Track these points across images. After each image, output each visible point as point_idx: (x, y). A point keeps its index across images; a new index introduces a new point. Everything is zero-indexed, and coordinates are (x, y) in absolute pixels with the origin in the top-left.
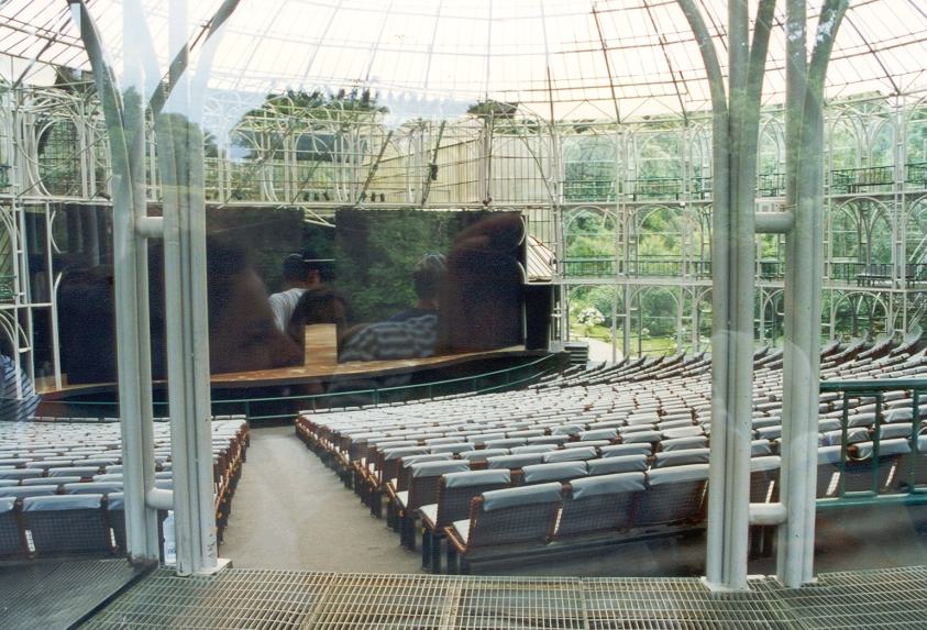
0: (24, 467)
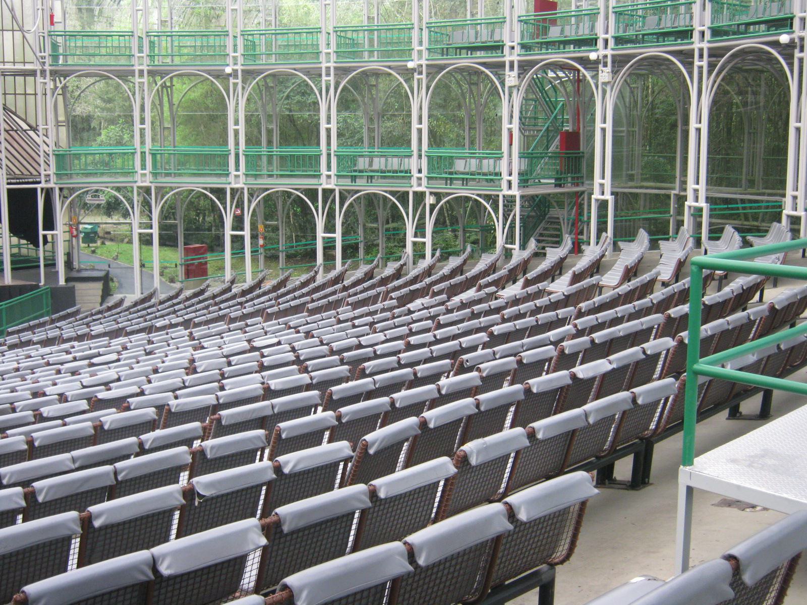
0: (17, 391)
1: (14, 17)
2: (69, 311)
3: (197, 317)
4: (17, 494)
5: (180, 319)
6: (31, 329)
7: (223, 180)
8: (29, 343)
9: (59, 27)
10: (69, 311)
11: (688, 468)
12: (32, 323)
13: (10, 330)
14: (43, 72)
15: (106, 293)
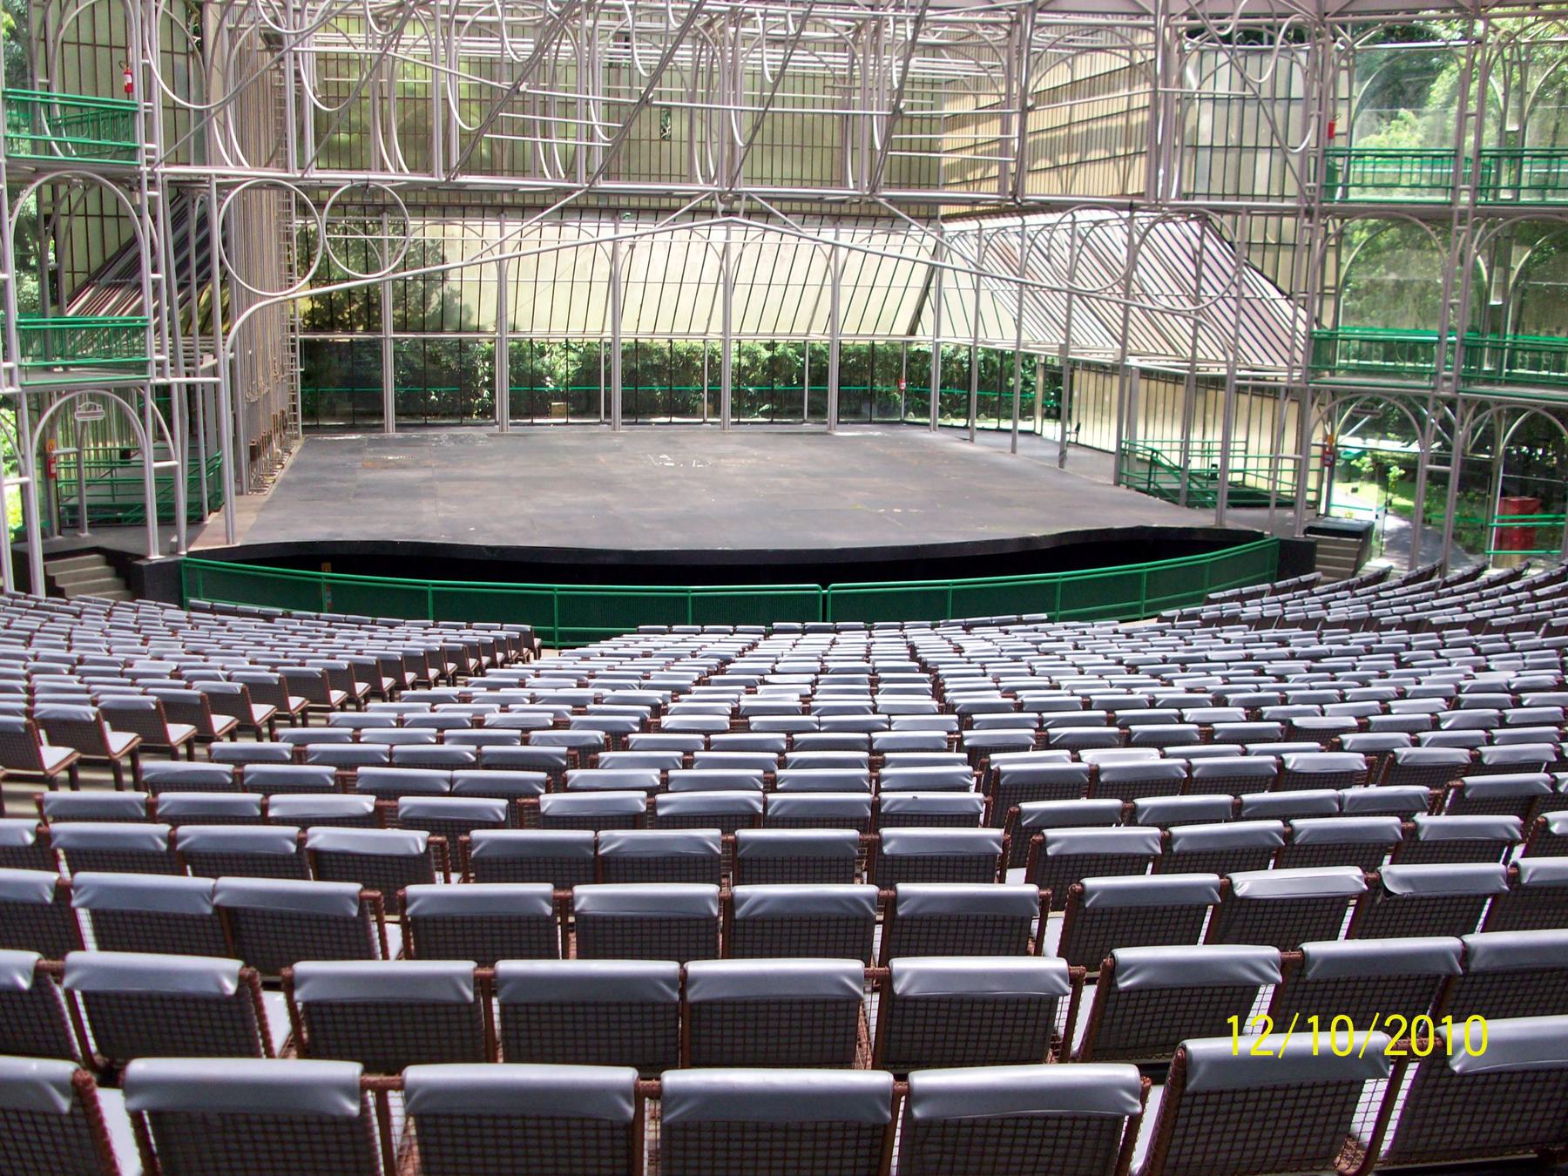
1: (1274, 132)
2: (1304, 578)
3: (1495, 617)
4: (1152, 837)
5: (1468, 617)
6: (1242, 598)
8: (1234, 619)
9: (1340, 143)
10: (1304, 578)
11: (1476, 959)
12: (1245, 590)
13: (1212, 596)
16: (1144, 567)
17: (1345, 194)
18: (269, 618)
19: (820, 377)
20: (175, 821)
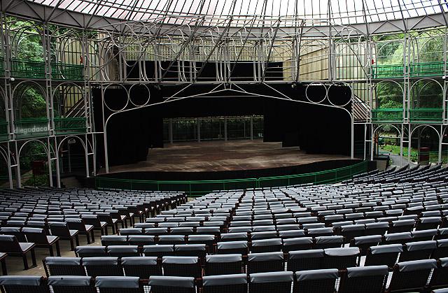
7: (439, 122)
14: (369, 81)
15: (388, 165)
16: (190, 182)
17: (376, 76)
18: (118, 192)
19: (223, 127)
20: (283, 238)
